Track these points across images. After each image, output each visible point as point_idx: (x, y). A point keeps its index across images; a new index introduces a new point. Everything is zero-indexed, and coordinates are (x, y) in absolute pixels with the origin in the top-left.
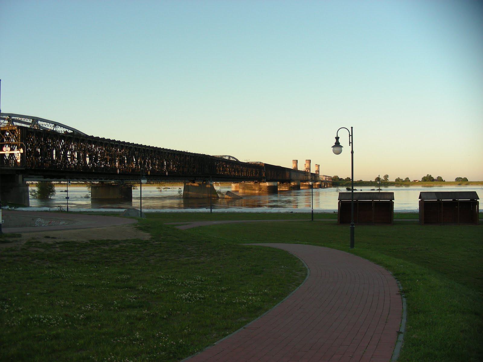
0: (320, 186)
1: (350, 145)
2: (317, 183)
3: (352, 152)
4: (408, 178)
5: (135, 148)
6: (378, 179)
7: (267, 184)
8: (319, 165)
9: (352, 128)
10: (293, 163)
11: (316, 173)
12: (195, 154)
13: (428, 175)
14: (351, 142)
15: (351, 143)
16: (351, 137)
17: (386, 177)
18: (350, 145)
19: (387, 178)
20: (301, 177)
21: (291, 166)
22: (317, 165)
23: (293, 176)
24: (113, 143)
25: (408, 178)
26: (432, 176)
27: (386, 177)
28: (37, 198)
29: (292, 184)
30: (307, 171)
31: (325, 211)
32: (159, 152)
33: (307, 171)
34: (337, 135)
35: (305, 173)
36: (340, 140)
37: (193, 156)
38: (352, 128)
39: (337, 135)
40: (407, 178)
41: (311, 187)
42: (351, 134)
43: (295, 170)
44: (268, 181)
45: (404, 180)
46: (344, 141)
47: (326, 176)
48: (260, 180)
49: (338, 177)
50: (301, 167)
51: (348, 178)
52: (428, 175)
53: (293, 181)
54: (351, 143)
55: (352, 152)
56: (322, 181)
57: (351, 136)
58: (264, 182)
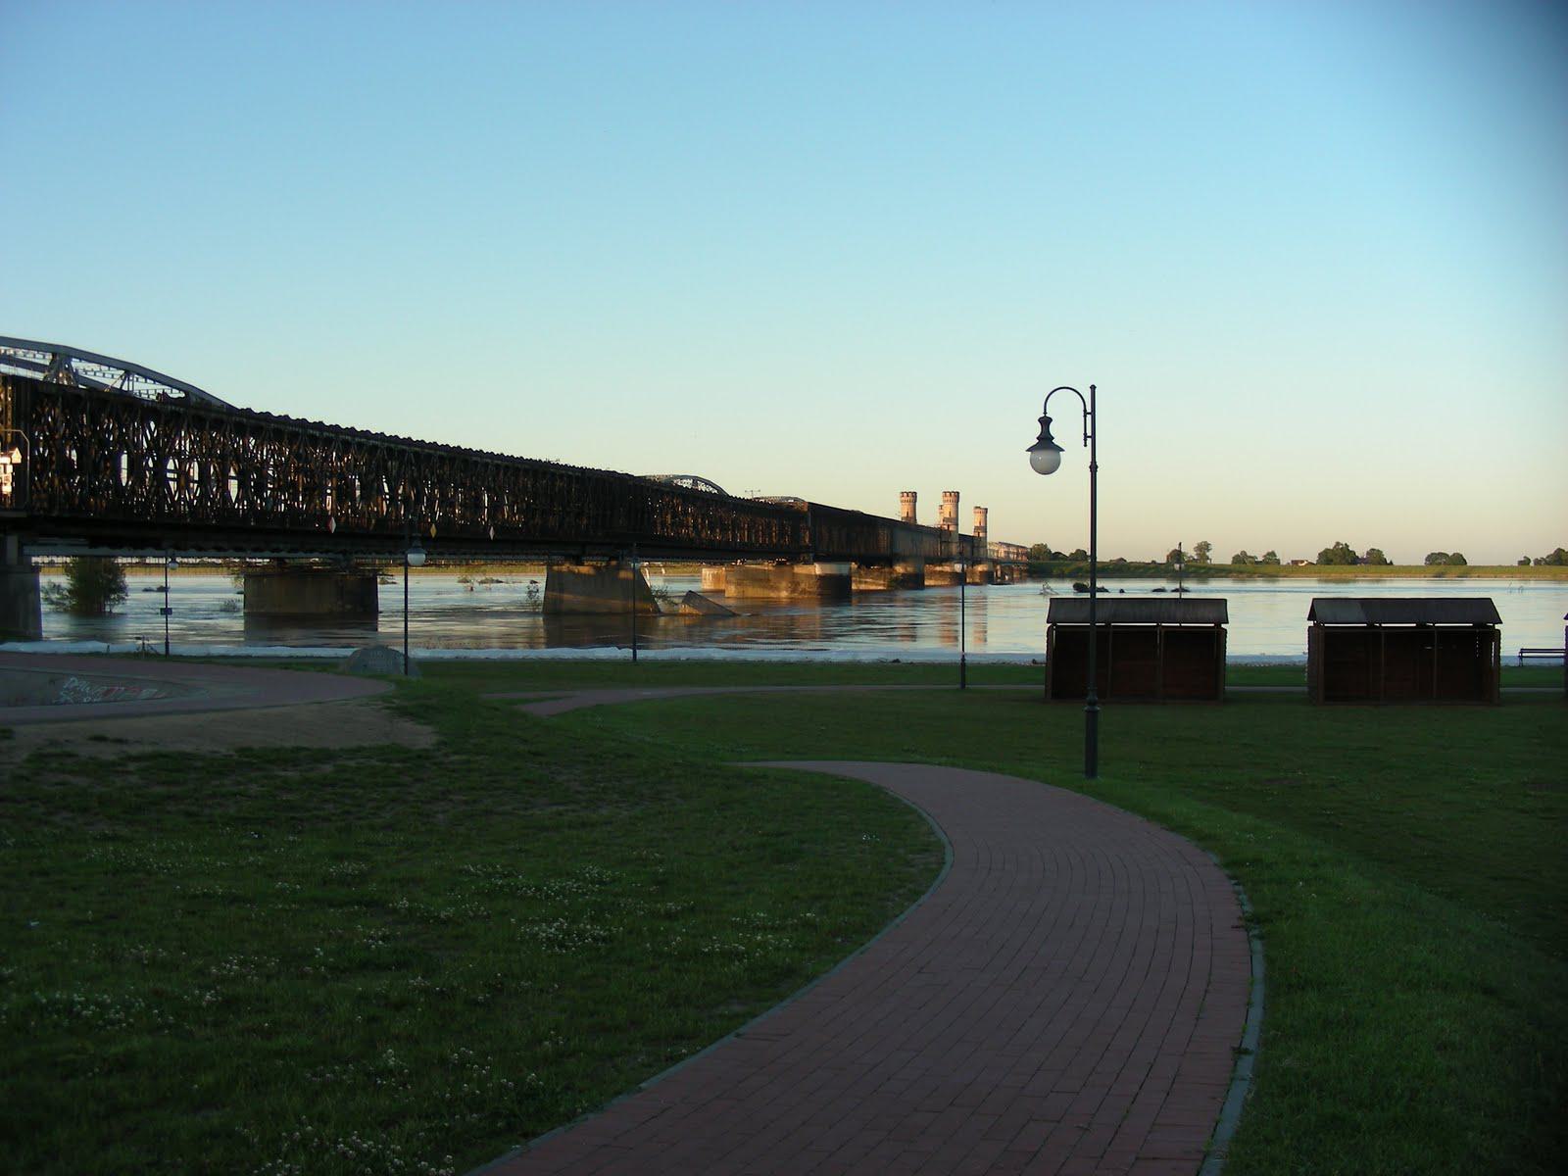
0: (989, 578)
1: (1085, 445)
2: (980, 568)
3: (1094, 468)
4: (1273, 554)
5: (389, 450)
6: (1177, 555)
7: (818, 569)
8: (986, 509)
9: (1093, 388)
10: (902, 502)
11: (976, 534)
12: (583, 470)
13: (1338, 544)
14: (1089, 433)
15: (1091, 437)
16: (1089, 417)
17: (1203, 548)
18: (1085, 445)
19: (1204, 554)
20: (928, 546)
21: (894, 511)
22: (978, 510)
23: (903, 544)
24: (349, 438)
25: (1273, 554)
26: (1350, 549)
27: (1203, 548)
28: (66, 611)
29: (899, 569)
30: (946, 527)
31: (1239, 661)
32: (466, 461)
33: (946, 527)
34: (1045, 413)
35: (940, 534)
36: (1053, 429)
37: (577, 478)
38: (1093, 388)
39: (1045, 413)
40: (1269, 554)
41: (960, 579)
42: (1089, 410)
43: (909, 526)
44: (818, 559)
45: (1260, 559)
46: (1067, 431)
47: (1009, 545)
48: (792, 554)
49: (1049, 547)
50: (929, 516)
51: (1078, 550)
52: (1338, 544)
53: (903, 559)
54: (1091, 437)
55: (1094, 468)
56: (995, 562)
57: (1091, 413)
58: (806, 563)
